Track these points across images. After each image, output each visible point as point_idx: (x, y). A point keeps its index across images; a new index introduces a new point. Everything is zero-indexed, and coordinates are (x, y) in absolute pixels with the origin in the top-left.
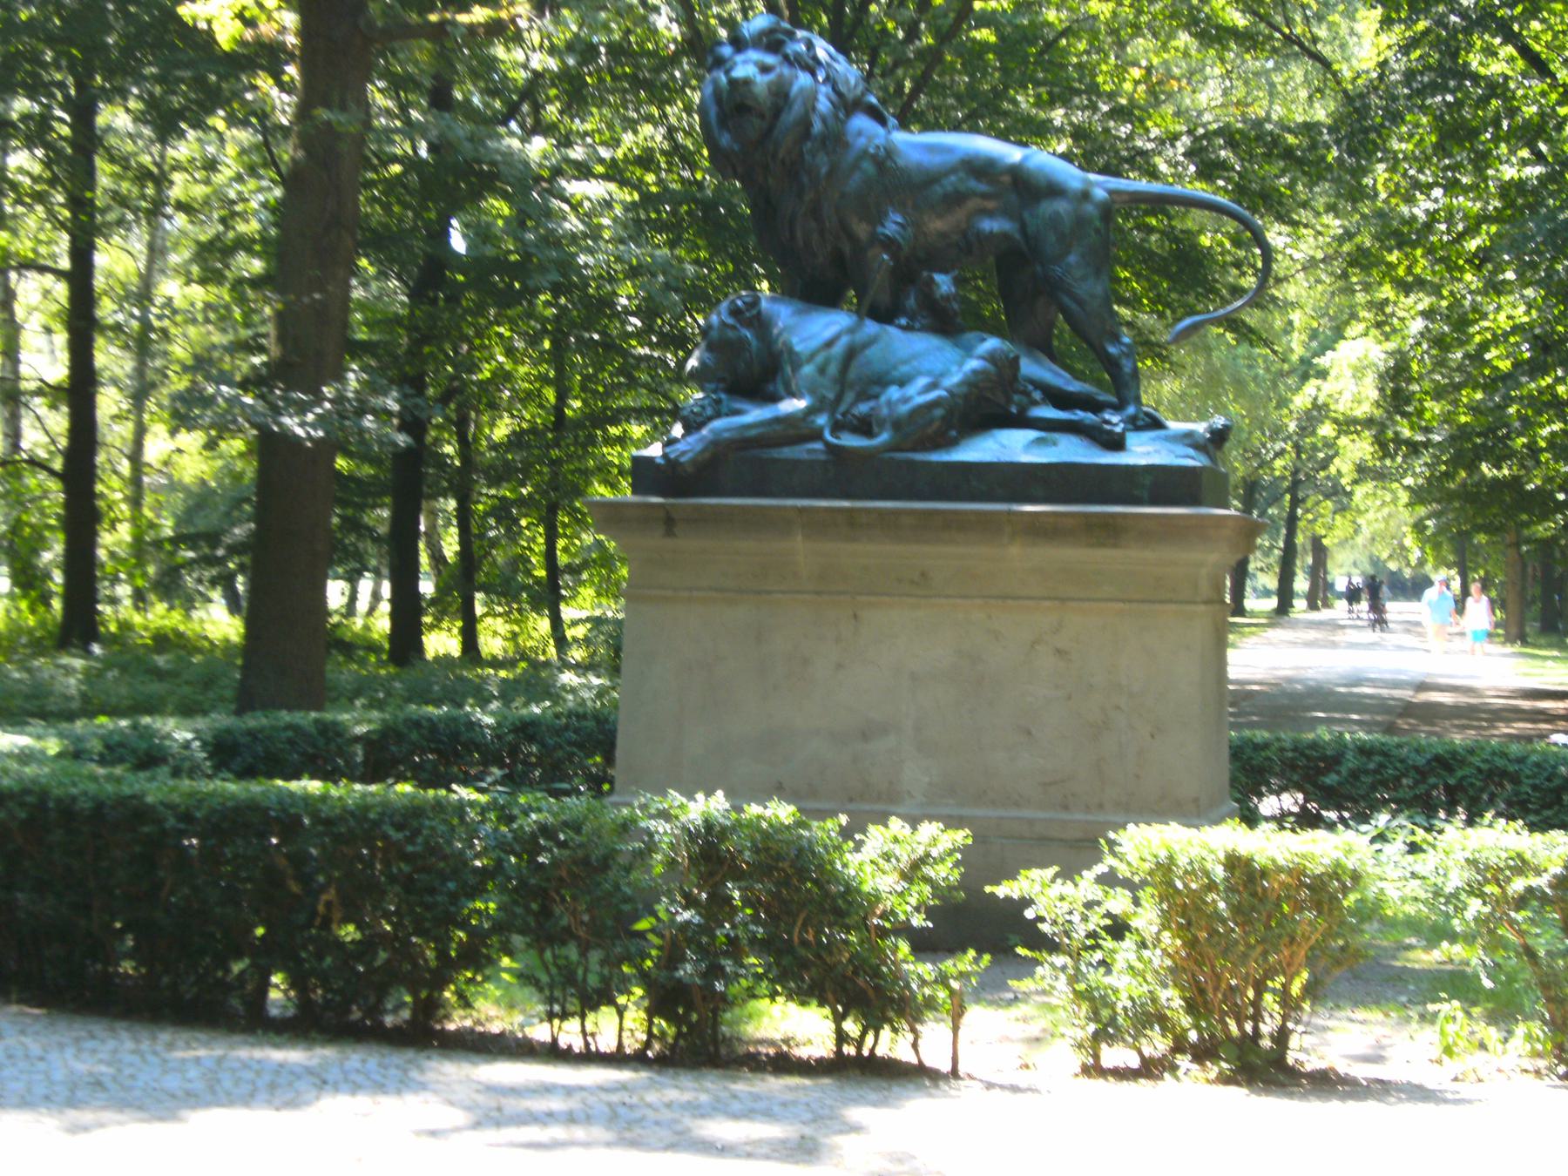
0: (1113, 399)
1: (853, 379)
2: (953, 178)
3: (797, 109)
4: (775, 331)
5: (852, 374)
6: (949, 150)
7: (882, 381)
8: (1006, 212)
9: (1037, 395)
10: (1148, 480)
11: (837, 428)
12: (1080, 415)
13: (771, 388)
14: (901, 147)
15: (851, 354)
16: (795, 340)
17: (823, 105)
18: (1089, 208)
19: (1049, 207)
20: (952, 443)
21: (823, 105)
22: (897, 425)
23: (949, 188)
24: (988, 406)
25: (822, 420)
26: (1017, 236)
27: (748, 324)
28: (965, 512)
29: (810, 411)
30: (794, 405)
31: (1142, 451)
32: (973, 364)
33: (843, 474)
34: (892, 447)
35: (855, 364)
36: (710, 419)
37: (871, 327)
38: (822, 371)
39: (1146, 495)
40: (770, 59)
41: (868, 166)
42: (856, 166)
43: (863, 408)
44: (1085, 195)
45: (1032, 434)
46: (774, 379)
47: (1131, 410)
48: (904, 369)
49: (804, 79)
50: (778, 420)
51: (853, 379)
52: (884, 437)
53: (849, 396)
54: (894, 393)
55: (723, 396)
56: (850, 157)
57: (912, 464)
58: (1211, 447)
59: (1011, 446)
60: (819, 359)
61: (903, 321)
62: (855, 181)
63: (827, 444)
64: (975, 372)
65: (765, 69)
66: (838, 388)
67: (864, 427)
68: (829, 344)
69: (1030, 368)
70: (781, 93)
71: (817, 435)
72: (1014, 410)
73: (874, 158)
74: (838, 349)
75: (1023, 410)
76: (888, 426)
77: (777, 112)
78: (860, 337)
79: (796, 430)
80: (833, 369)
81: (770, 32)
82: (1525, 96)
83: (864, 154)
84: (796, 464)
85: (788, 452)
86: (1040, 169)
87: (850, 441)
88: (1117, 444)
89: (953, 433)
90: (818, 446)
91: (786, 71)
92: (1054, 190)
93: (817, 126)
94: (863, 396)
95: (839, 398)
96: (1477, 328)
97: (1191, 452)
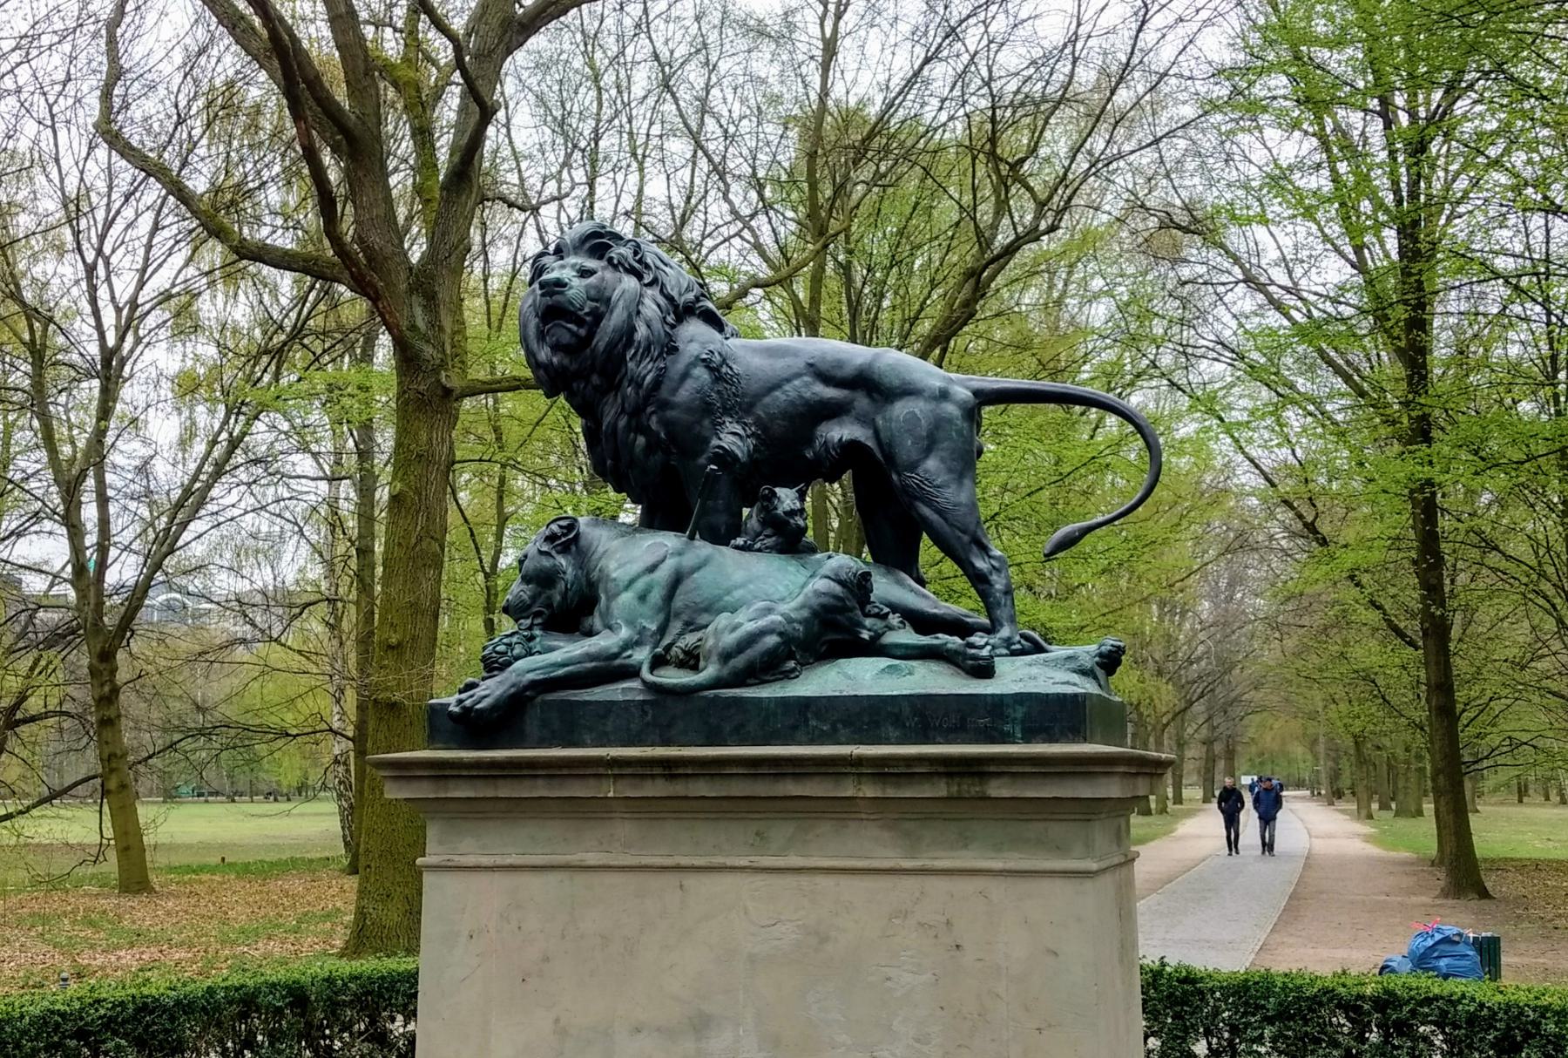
0: (985, 620)
1: (675, 602)
2: (796, 382)
4: (596, 556)
5: (678, 602)
7: (712, 608)
9: (895, 619)
10: (1020, 712)
11: (658, 662)
12: (943, 639)
13: (589, 621)
14: (740, 353)
15: (677, 580)
16: (612, 565)
17: (650, 309)
18: (950, 409)
19: (901, 409)
20: (788, 676)
21: (650, 309)
22: (726, 657)
23: (793, 394)
24: (834, 630)
25: (642, 655)
27: (565, 549)
28: (977, 742)
29: (628, 645)
30: (604, 642)
31: (1015, 677)
32: (821, 584)
33: (667, 712)
34: (718, 683)
35: (681, 589)
36: (509, 664)
37: (703, 548)
38: (642, 598)
40: (591, 264)
41: (701, 373)
42: (685, 375)
43: (690, 639)
44: (944, 395)
45: (884, 662)
46: (591, 613)
47: (1005, 632)
48: (737, 594)
49: (630, 282)
50: (590, 657)
51: (675, 602)
52: (710, 671)
53: (676, 627)
54: (723, 620)
55: (537, 632)
58: (1100, 673)
60: (640, 585)
61: (740, 541)
63: (644, 682)
64: (818, 594)
65: (584, 273)
66: (661, 617)
67: (691, 660)
68: (652, 568)
69: (885, 587)
70: (602, 300)
71: (632, 672)
72: (865, 635)
73: (707, 363)
74: (663, 573)
75: (877, 636)
76: (714, 658)
77: (598, 317)
78: (688, 560)
79: (610, 670)
80: (656, 596)
81: (1401, 1034)
84: (609, 707)
86: (893, 368)
87: (672, 677)
88: (984, 670)
89: (792, 664)
90: (635, 684)
91: (609, 275)
93: (642, 332)
94: (691, 626)
95: (662, 630)
97: (1075, 678)
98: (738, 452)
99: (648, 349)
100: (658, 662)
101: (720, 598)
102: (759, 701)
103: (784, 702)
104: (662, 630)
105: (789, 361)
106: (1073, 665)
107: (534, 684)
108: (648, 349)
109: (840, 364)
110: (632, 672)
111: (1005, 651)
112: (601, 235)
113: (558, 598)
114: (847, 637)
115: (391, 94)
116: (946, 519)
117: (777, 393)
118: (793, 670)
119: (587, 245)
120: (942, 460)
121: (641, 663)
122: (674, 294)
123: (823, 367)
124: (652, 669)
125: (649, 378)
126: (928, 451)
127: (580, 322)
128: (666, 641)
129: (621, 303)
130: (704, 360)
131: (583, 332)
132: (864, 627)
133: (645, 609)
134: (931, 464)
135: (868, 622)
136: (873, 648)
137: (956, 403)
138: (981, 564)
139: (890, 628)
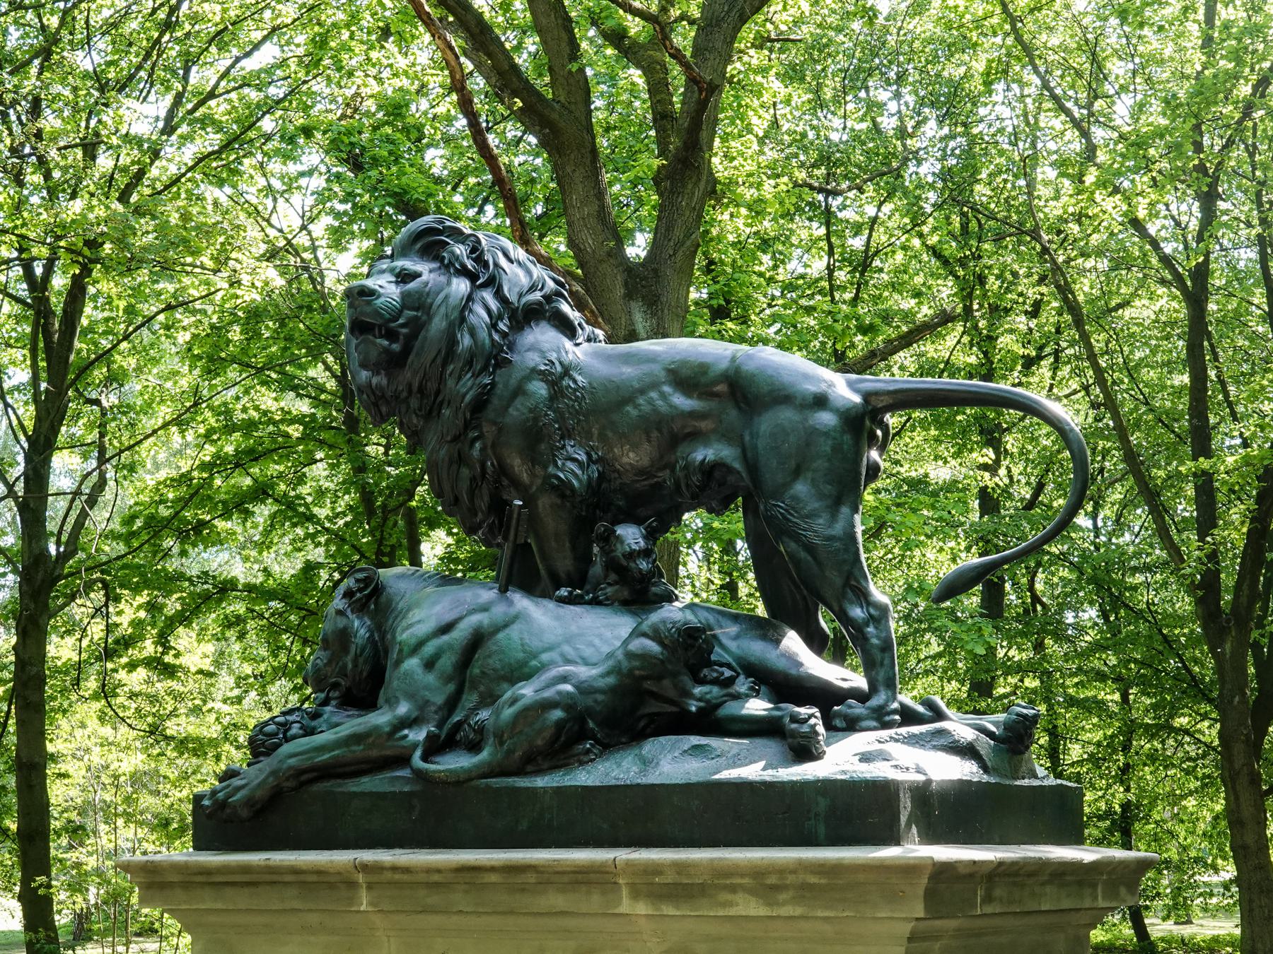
3: (438, 324)
6: (651, 358)
8: (727, 436)
9: (742, 685)
10: (823, 804)
11: (434, 748)
19: (767, 422)
21: (479, 315)
23: (646, 408)
26: (737, 465)
28: (295, 871)
39: (822, 830)
41: (539, 389)
53: (470, 699)
56: (516, 375)
57: (488, 786)
59: (671, 763)
60: (429, 649)
62: (517, 411)
63: (419, 774)
66: (451, 687)
68: (447, 628)
74: (461, 633)
77: (417, 327)
80: (447, 662)
82: (369, 33)
83: (535, 373)
85: (368, 784)
90: (405, 773)
92: (779, 395)
96: (660, 403)
98: (575, 483)
99: (470, 363)
100: (434, 748)
101: (524, 663)
102: (534, 791)
103: (559, 791)
104: (452, 703)
105: (646, 368)
106: (943, 741)
107: (298, 772)
108: (470, 363)
109: (703, 368)
110: (403, 760)
111: (874, 724)
112: (439, 232)
113: (350, 666)
114: (674, 709)
115: (1260, 329)
116: (815, 558)
117: (629, 408)
118: (588, 751)
119: (418, 246)
120: (814, 483)
121: (415, 746)
122: (513, 297)
123: (685, 372)
124: (425, 758)
125: (468, 398)
126: (797, 473)
127: (391, 335)
128: (456, 718)
129: (443, 310)
130: (542, 373)
131: (396, 347)
132: (691, 696)
133: (431, 678)
134: (801, 488)
135: (698, 690)
136: (711, 723)
137: (836, 411)
138: (857, 612)
139: (737, 697)
